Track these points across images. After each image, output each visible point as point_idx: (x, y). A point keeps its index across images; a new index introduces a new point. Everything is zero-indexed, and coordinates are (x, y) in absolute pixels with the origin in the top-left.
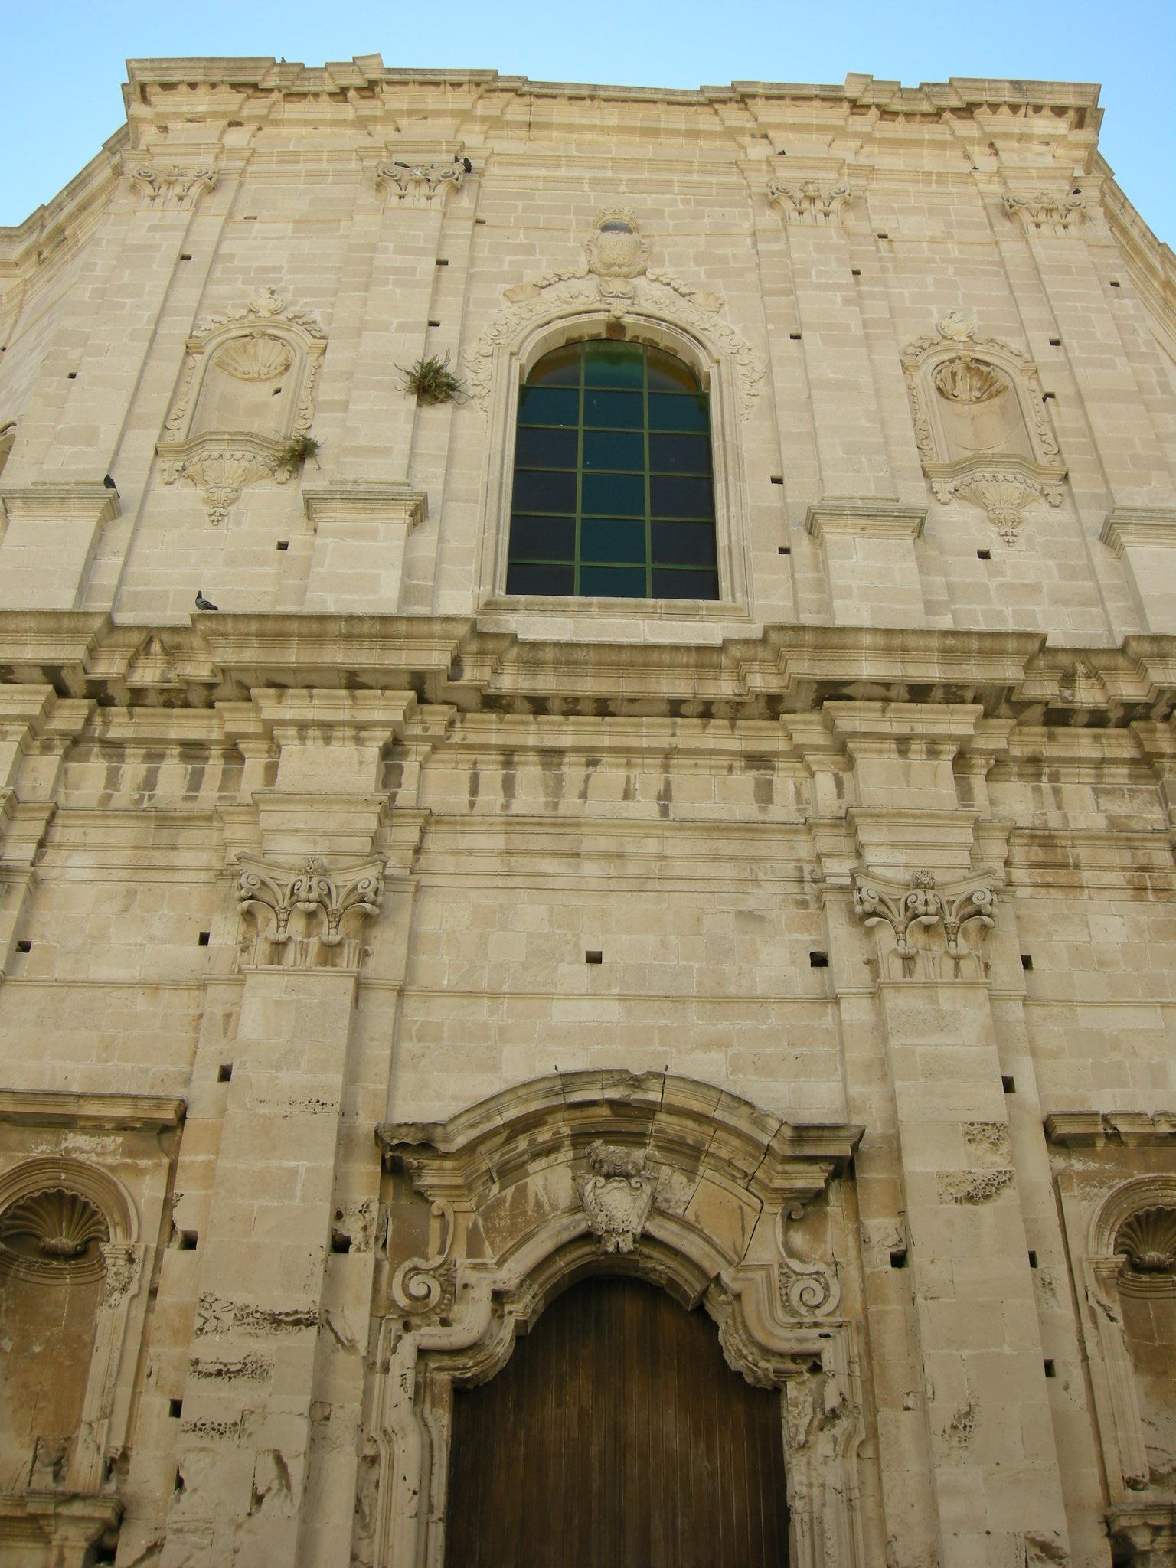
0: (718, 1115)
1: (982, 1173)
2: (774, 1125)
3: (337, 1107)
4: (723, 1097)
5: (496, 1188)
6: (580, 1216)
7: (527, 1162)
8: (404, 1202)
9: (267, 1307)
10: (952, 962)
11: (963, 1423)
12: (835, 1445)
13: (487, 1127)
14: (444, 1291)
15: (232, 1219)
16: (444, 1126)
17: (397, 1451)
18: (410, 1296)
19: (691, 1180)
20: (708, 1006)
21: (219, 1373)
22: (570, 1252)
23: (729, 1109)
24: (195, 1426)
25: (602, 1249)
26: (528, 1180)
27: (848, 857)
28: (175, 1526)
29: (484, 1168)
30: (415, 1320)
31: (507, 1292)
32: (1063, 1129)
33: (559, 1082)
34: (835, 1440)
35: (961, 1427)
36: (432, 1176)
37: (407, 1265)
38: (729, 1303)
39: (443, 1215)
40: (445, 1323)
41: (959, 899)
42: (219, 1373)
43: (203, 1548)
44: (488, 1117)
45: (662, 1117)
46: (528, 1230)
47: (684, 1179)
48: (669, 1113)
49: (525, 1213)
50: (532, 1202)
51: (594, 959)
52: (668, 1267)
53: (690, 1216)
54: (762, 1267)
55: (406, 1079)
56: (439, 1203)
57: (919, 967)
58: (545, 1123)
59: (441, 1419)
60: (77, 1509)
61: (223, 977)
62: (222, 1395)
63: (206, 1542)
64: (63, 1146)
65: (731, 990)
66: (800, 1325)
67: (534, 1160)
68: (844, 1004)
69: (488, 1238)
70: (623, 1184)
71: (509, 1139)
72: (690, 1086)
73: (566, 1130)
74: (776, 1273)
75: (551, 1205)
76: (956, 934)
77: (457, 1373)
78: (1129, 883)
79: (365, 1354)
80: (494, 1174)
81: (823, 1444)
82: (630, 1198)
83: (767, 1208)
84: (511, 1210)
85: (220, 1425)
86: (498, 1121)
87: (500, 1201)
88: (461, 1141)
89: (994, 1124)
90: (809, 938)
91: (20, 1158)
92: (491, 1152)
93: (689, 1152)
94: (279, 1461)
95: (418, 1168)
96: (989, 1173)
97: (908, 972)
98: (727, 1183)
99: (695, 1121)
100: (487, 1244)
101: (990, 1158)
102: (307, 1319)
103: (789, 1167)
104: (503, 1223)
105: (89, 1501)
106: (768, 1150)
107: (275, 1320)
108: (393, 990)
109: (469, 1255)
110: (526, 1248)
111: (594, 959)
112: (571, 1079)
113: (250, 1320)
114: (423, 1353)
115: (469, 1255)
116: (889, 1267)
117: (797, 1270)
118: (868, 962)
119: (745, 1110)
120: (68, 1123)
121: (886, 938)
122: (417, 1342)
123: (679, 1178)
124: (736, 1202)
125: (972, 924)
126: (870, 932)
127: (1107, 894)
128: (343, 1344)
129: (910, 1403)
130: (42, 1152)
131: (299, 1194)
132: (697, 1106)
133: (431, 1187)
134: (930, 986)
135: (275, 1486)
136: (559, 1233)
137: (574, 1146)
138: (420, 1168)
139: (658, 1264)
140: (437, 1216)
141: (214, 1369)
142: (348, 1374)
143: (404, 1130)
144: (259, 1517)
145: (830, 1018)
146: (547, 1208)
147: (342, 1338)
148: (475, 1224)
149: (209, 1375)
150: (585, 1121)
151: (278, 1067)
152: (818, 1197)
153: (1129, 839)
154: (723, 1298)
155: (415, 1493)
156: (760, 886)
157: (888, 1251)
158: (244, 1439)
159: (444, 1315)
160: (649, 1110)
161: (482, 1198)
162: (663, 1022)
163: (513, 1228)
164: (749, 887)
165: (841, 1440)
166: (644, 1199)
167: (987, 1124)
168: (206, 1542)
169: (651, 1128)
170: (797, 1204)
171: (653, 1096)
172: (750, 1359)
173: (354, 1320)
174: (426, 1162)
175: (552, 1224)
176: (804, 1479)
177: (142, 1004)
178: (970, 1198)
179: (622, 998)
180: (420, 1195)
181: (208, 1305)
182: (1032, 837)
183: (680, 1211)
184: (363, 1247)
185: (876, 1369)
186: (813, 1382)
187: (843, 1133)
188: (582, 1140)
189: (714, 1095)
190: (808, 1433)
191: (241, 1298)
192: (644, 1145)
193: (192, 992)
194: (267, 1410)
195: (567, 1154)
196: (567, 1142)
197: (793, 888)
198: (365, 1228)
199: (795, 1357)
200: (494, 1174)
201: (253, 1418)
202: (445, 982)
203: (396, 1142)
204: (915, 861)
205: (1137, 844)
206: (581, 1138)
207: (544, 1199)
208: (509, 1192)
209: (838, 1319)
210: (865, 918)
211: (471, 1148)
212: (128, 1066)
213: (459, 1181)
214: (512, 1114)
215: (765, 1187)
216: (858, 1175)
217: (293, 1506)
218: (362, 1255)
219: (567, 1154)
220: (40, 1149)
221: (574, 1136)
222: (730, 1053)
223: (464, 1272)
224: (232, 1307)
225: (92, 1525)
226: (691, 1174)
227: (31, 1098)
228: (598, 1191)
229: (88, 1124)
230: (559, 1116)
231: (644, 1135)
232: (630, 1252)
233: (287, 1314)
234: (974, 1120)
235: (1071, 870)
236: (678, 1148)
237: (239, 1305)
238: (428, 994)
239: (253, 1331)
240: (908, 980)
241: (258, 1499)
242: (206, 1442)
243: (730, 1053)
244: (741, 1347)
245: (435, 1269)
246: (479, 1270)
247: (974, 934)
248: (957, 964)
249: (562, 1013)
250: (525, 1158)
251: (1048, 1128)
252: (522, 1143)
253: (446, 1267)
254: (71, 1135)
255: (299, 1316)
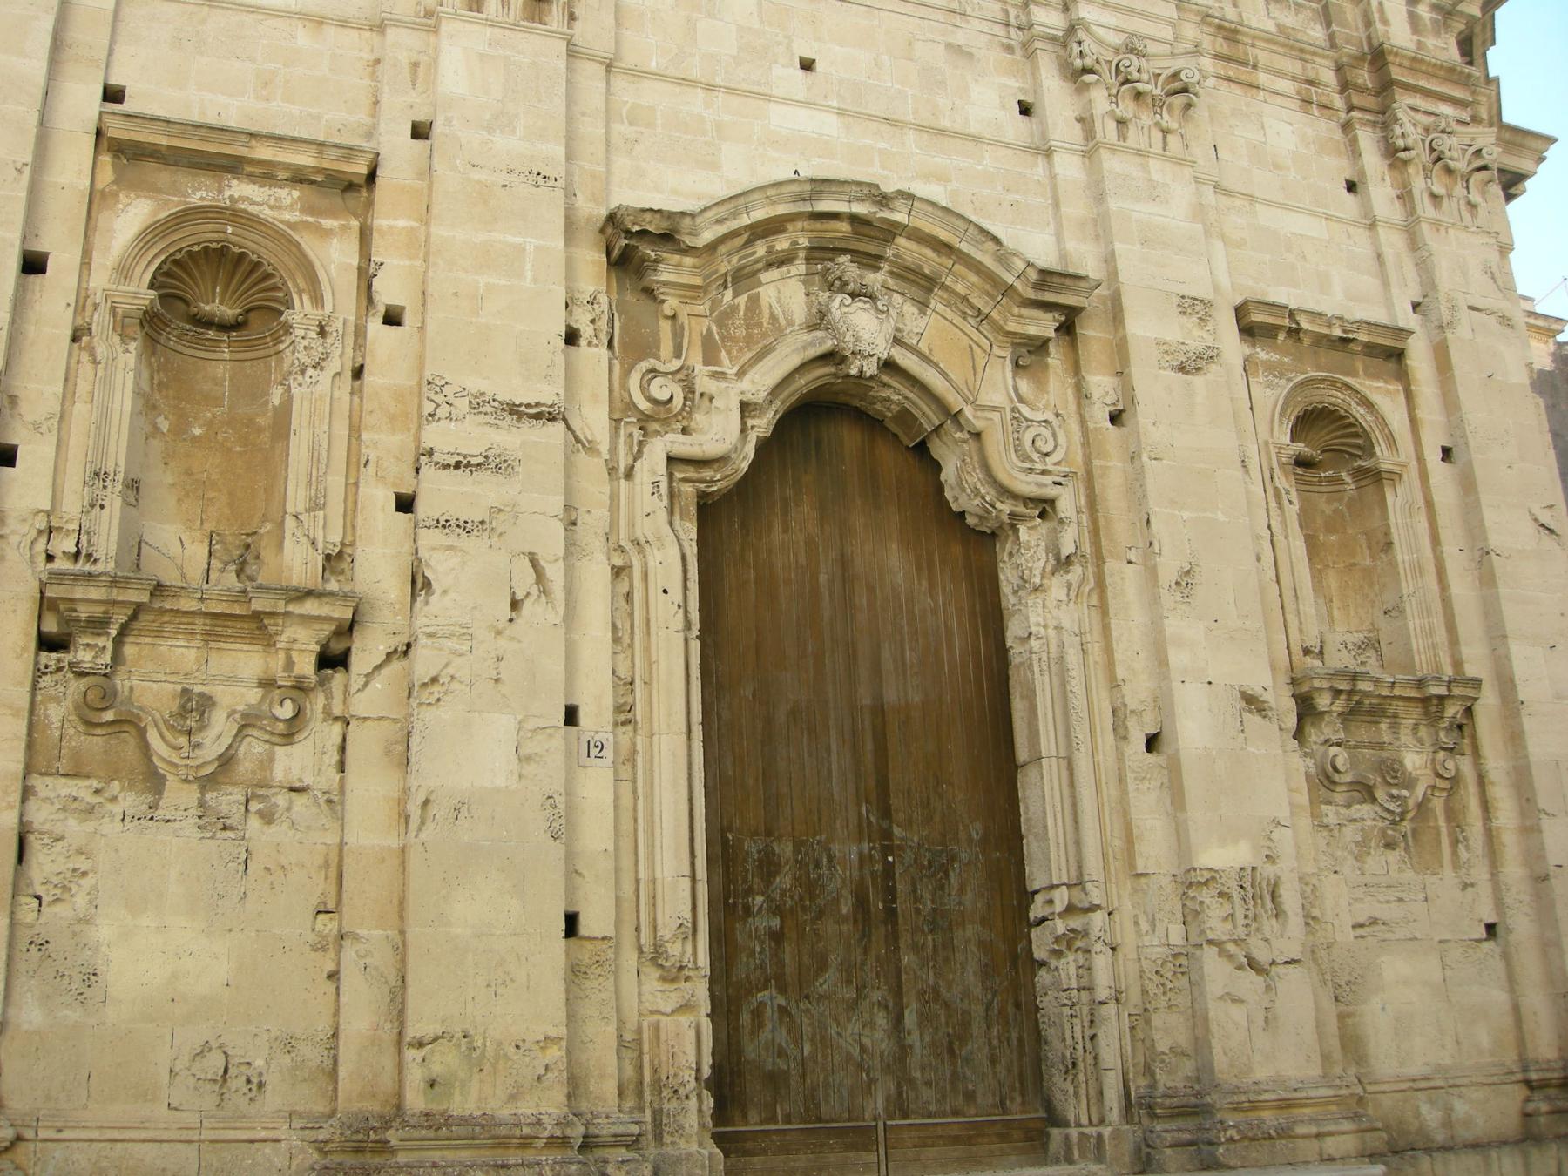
0: (964, 247)
1: (1195, 345)
2: (1021, 266)
3: (561, 183)
4: (971, 229)
5: (729, 294)
6: (820, 334)
7: (759, 271)
8: (630, 297)
9: (505, 396)
10: (1160, 135)
11: (1185, 580)
12: (1069, 590)
13: (734, 225)
14: (685, 399)
15: (455, 294)
16: (693, 216)
17: (651, 564)
18: (655, 402)
19: (923, 313)
20: (925, 136)
21: (457, 465)
22: (809, 372)
23: (975, 243)
24: (438, 521)
25: (845, 371)
26: (760, 290)
27: (1055, 9)
28: (428, 630)
29: (723, 270)
30: (655, 426)
31: (756, 404)
32: (1257, 317)
33: (808, 187)
34: (1069, 586)
35: (1184, 584)
36: (670, 271)
37: (644, 365)
38: (965, 441)
39: (674, 317)
40: (685, 431)
41: (1166, 73)
42: (457, 465)
43: (461, 655)
44: (735, 215)
45: (901, 241)
46: (766, 342)
47: (916, 311)
48: (909, 238)
49: (760, 325)
50: (766, 314)
51: (807, 65)
52: (906, 398)
53: (923, 347)
54: (994, 409)
55: (621, 163)
56: (671, 303)
57: (1132, 131)
58: (784, 230)
59: (689, 531)
60: (310, 607)
61: (407, 19)
62: (465, 489)
63: (465, 648)
64: (227, 193)
65: (945, 123)
66: (1031, 470)
67: (767, 270)
68: (1057, 157)
69: (724, 346)
70: (868, 305)
71: (749, 243)
72: (939, 213)
73: (804, 242)
74: (1009, 418)
75: (786, 320)
76: (1161, 107)
77: (702, 486)
78: (1298, 93)
79: (607, 457)
80: (729, 279)
81: (1057, 588)
82: (876, 321)
83: (996, 351)
84: (745, 320)
85: (466, 522)
86: (745, 220)
87: (734, 309)
88: (707, 236)
89: (1202, 301)
90: (1017, 85)
91: (175, 204)
92: (730, 254)
93: (922, 282)
94: (534, 562)
95: (656, 261)
96: (1200, 347)
97: (1122, 136)
98: (958, 320)
99: (934, 250)
100: (723, 353)
101: (1197, 332)
102: (550, 413)
103: (1025, 312)
104: (738, 332)
105: (325, 600)
106: (1008, 290)
107: (514, 410)
108: (601, 63)
109: (706, 363)
110: (768, 362)
111: (807, 65)
112: (821, 185)
113: (487, 408)
114: (672, 460)
115: (706, 363)
116: (1108, 424)
117: (1028, 416)
118: (1080, 120)
119: (991, 246)
120: (232, 166)
121: (1099, 100)
122: (669, 449)
123: (910, 309)
124: (967, 341)
125: (1179, 100)
126: (1083, 89)
127: (1279, 100)
128: (584, 446)
129: (1132, 556)
130: (202, 199)
131: (529, 274)
132: (943, 235)
133: (665, 284)
134: (1142, 154)
135: (535, 590)
136: (804, 348)
137: (807, 259)
138: (657, 261)
139: (895, 394)
140: (667, 317)
141: (452, 460)
142: (591, 470)
143: (648, 216)
144: (519, 622)
145: (1040, 170)
146: (782, 322)
147: (582, 437)
148: (709, 329)
149: (446, 466)
150: (823, 234)
151: (490, 129)
152: (1039, 347)
153: (1302, 50)
154: (958, 435)
155: (679, 606)
156: (968, 22)
157: (1108, 409)
158: (495, 539)
159: (685, 423)
160: (890, 232)
161: (715, 304)
162: (882, 145)
163: (749, 340)
164: (958, 20)
165: (1075, 586)
166: (889, 328)
167: (1196, 299)
168: (464, 648)
169: (889, 252)
170: (1024, 350)
171: (900, 217)
172: (987, 499)
173: (594, 419)
174: (665, 255)
175: (789, 339)
176: (1040, 620)
177: (303, 38)
178: (1182, 369)
179: (840, 113)
180: (649, 292)
181: (437, 389)
182: (1220, 27)
183: (914, 342)
184: (595, 341)
185: (1102, 522)
186: (1043, 527)
187: (1083, 284)
188: (817, 255)
189: (961, 225)
190: (1043, 577)
191: (475, 384)
192: (877, 269)
193: (362, 32)
194: (517, 509)
195: (799, 267)
196: (802, 255)
197: (999, 30)
198: (593, 321)
199: (1028, 501)
200: (729, 279)
201: (501, 516)
202: (654, 64)
203: (636, 228)
204: (1124, 26)
205: (1307, 57)
206: (820, 252)
207: (778, 312)
208: (742, 300)
209: (1064, 469)
210: (1078, 75)
211: (712, 247)
212: (295, 109)
213: (698, 281)
214: (759, 214)
215: (999, 329)
216: (1078, 331)
217: (557, 613)
218: (595, 349)
219: (799, 267)
220: (198, 195)
221: (811, 249)
222: (949, 188)
223: (703, 383)
224: (464, 393)
225: (326, 626)
226: (923, 305)
227: (190, 131)
228: (845, 309)
229: (258, 170)
230: (799, 225)
231: (880, 258)
232: (872, 377)
233: (528, 406)
234: (1186, 293)
235: (1250, 69)
236: (912, 277)
237: (474, 391)
238: (638, 74)
239: (493, 421)
240: (1121, 143)
241: (515, 605)
242: (452, 540)
243: (949, 188)
244: (979, 486)
245: (673, 373)
246: (717, 379)
247: (1177, 112)
248: (1165, 138)
249: (783, 119)
250: (760, 266)
251: (1240, 311)
252: (760, 249)
253: (685, 372)
254: (235, 182)
255: (543, 409)
